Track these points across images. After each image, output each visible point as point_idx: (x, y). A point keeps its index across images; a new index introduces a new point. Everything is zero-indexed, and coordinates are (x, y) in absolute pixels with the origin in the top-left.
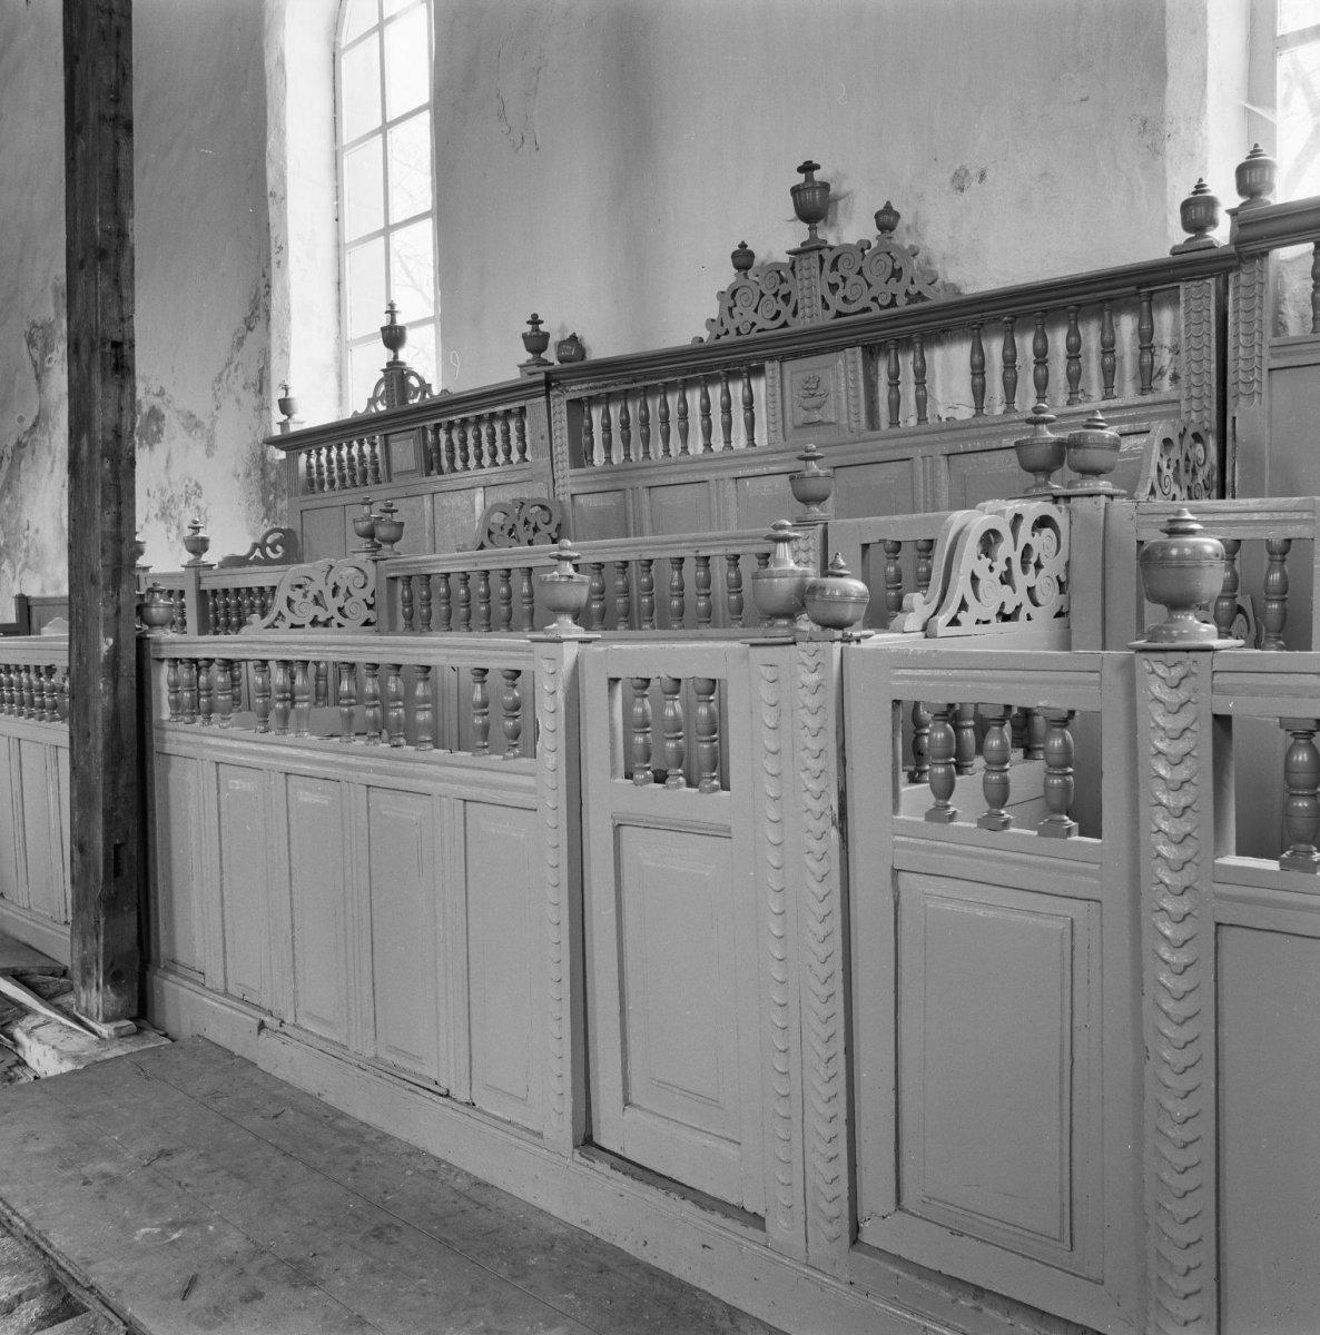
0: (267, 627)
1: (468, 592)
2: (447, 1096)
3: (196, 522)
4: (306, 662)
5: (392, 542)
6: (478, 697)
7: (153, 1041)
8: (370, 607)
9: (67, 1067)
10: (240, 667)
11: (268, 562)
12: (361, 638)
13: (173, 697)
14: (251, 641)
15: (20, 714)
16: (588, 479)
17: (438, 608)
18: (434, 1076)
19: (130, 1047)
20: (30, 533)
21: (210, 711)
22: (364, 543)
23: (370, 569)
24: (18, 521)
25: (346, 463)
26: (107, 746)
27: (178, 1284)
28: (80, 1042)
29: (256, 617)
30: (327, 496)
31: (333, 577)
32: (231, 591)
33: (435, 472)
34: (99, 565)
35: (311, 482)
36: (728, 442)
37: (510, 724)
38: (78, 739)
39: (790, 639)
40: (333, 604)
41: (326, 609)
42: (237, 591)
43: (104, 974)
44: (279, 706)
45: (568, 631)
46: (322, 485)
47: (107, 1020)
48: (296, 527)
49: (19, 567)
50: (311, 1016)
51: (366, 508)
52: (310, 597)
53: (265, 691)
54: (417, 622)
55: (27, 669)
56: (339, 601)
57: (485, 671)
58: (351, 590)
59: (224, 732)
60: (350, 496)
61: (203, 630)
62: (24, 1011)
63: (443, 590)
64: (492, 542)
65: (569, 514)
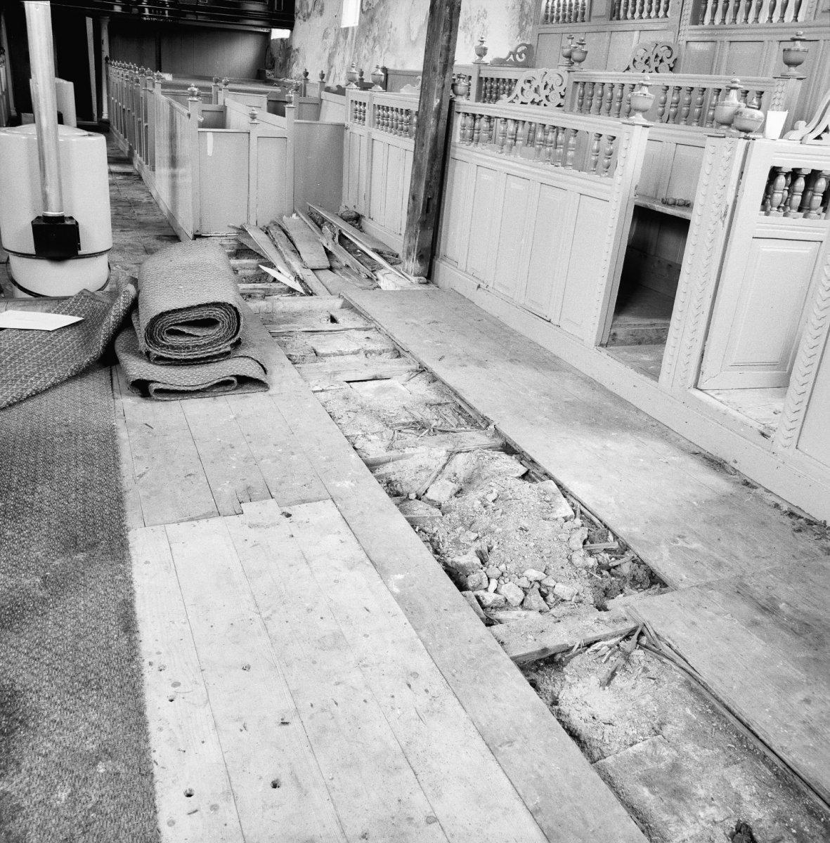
0: (510, 102)
1: (612, 95)
2: (549, 322)
3: (482, 38)
4: (524, 122)
5: (580, 61)
6: (595, 147)
7: (432, 287)
8: (562, 97)
9: (398, 289)
10: (494, 121)
11: (517, 65)
12: (556, 114)
13: (462, 132)
14: (502, 107)
15: (391, 132)
16: (700, 32)
17: (596, 102)
18: (546, 314)
19: (424, 287)
20: (392, 30)
21: (478, 141)
22: (566, 61)
23: (565, 75)
24: (386, 22)
25: (567, 7)
26: (431, 151)
27: (440, 356)
28: (403, 283)
29: (504, 96)
30: (554, 27)
31: (546, 79)
32: (495, 79)
33: (615, 18)
34: (439, 62)
35: (547, 17)
36: (782, 17)
37: (606, 161)
38: (419, 145)
39: (723, 135)
40: (543, 93)
41: (650, 67)
42: (498, 80)
43: (417, 255)
44: (509, 141)
45: (639, 121)
46: (552, 20)
47: (415, 275)
48: (534, 44)
49: (384, 50)
50: (500, 284)
51: (570, 41)
52: (533, 89)
53: (504, 134)
54: (584, 108)
55: (397, 110)
56: (547, 92)
57: (601, 135)
58: (554, 87)
59: (483, 151)
60: (567, 28)
61: (478, 99)
62: (381, 268)
63: (600, 92)
64: (635, 66)
65: (683, 54)
